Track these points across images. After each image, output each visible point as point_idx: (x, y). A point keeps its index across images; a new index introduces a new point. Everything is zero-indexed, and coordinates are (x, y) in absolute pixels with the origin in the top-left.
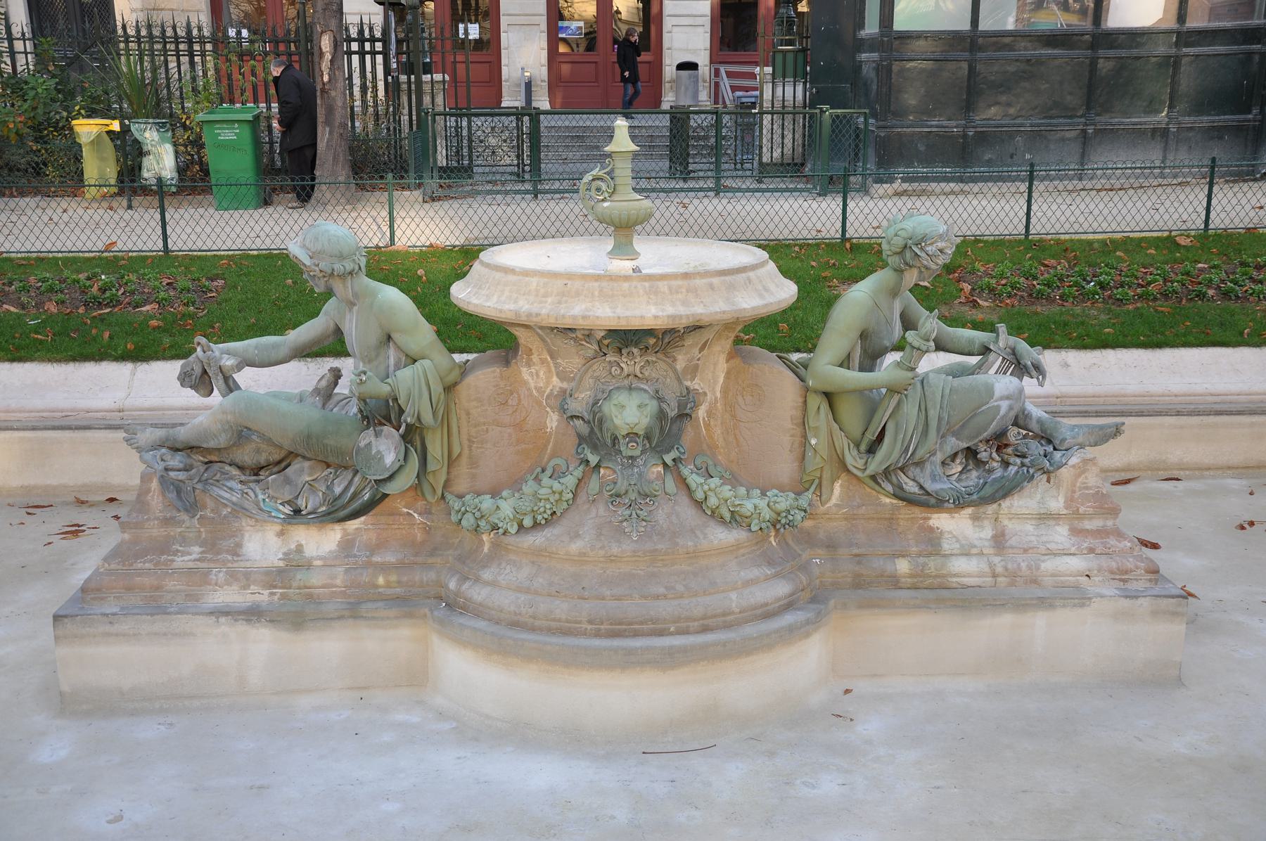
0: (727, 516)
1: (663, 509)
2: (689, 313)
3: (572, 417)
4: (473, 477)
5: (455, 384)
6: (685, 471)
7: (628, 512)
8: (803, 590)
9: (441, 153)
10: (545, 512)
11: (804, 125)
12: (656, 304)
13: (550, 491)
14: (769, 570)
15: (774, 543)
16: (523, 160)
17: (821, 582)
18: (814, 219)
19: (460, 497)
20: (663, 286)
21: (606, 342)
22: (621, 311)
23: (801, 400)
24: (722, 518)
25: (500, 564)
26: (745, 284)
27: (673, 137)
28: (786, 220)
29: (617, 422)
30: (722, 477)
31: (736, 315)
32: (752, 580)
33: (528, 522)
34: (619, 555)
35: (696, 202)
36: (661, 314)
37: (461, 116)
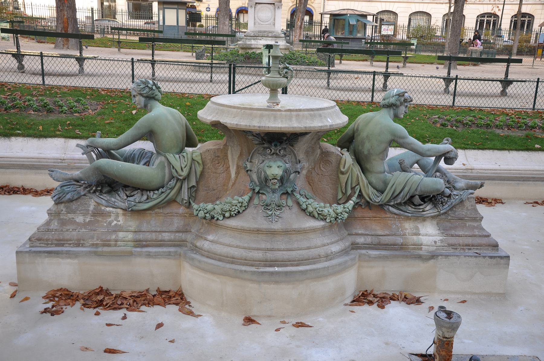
0: (316, 215)
10: (235, 211)
13: (237, 202)
33: (227, 215)
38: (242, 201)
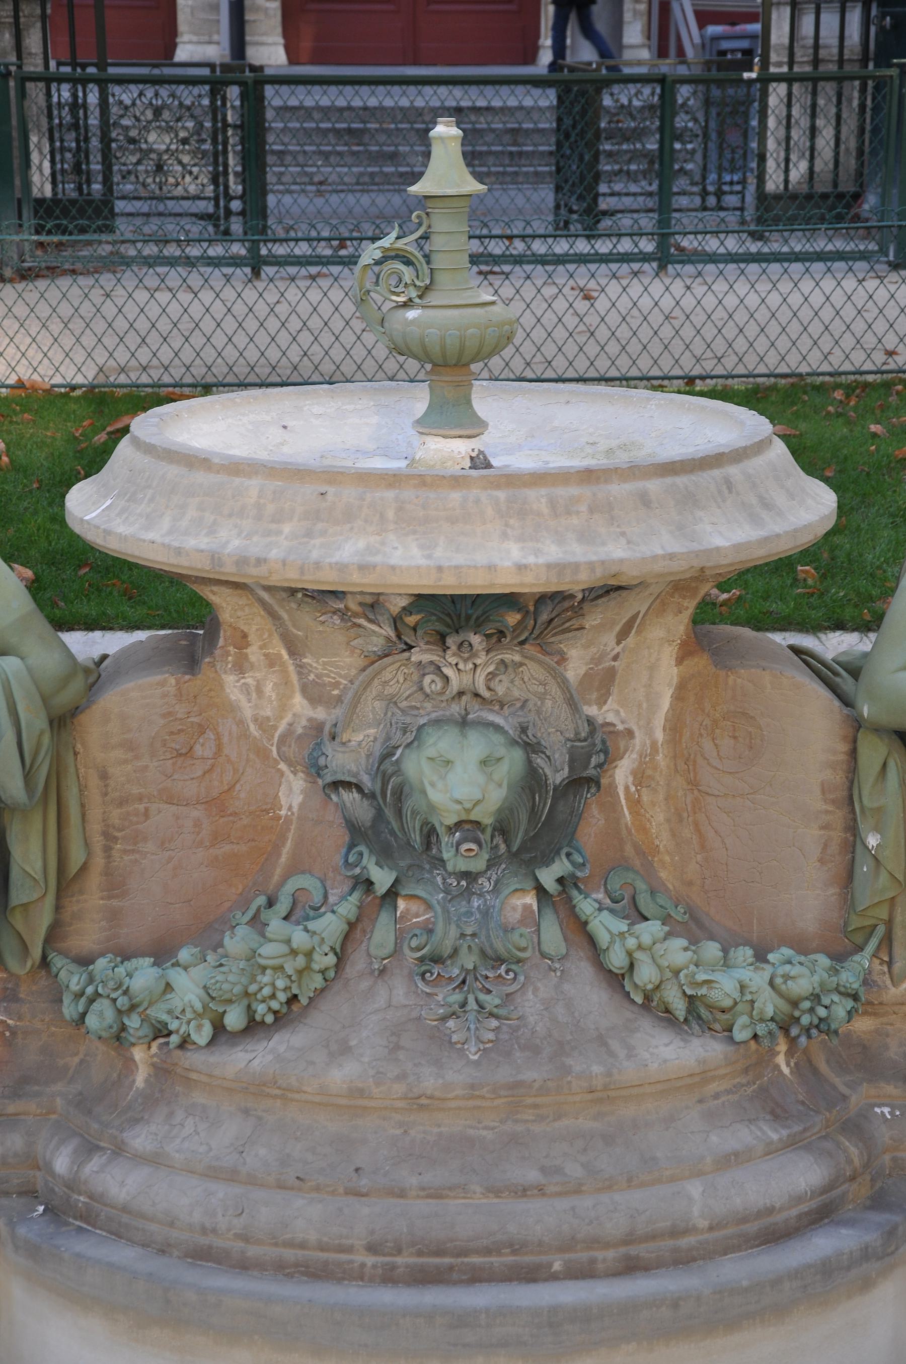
0: (679, 1007)
1: (536, 990)
2: (594, 558)
3: (336, 785)
4: (114, 917)
5: (75, 711)
6: (586, 906)
7: (457, 997)
8: (853, 1178)
9: (40, 168)
10: (273, 996)
11: (862, 107)
12: (521, 539)
13: (284, 949)
14: (776, 1130)
15: (786, 1070)
16: (227, 187)
17: (894, 1160)
18: (880, 326)
19: (85, 961)
20: (537, 497)
21: (411, 620)
22: (444, 555)
23: (843, 748)
24: (667, 1011)
25: (171, 1114)
26: (720, 492)
27: (563, 133)
28: (816, 328)
29: (435, 796)
30: (666, 919)
31: (697, 563)
32: (736, 1154)
33: (234, 1019)
34: (437, 1094)
35: (614, 289)
36: (531, 560)
37: (85, 81)
38: (308, 947)
